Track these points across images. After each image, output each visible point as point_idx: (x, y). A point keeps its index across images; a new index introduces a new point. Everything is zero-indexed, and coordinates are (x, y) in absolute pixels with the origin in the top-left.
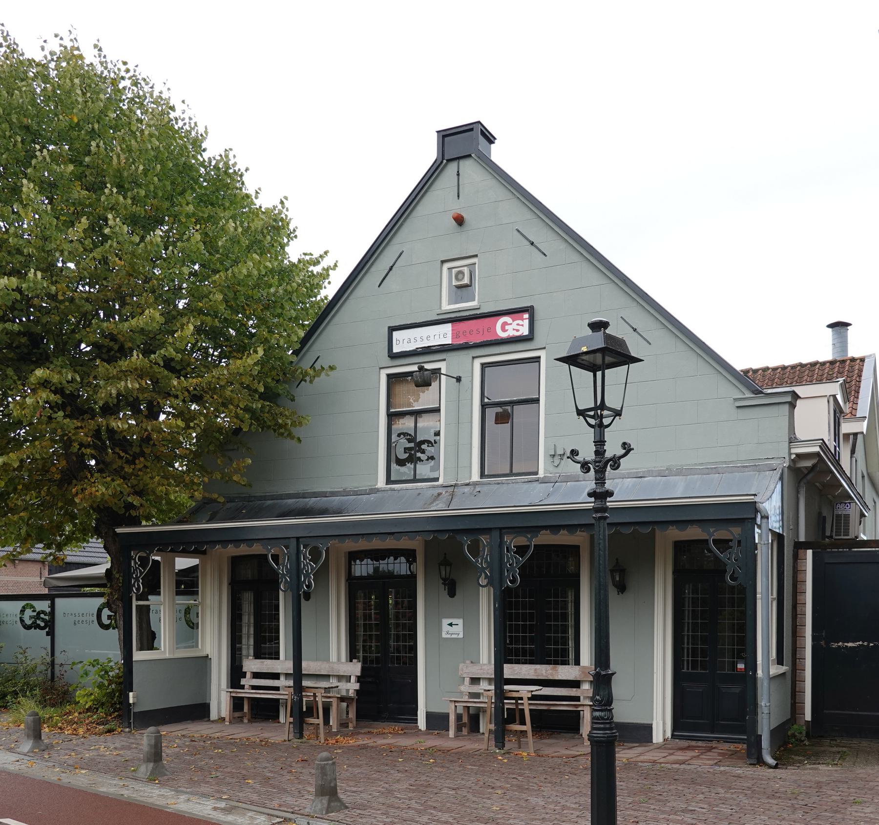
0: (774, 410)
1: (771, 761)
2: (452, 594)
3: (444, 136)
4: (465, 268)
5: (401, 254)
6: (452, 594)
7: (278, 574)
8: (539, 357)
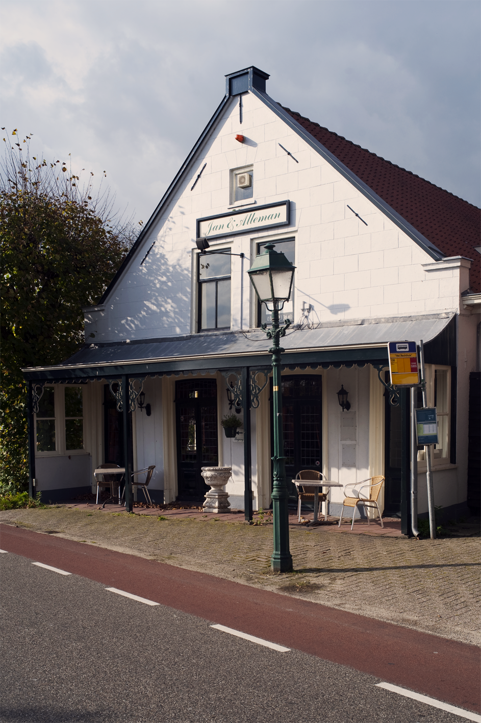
0: (449, 272)
1: (415, 533)
2: (149, 413)
3: (230, 80)
4: (246, 174)
5: (280, 145)
6: (149, 413)
7: (116, 400)
8: (294, 237)
